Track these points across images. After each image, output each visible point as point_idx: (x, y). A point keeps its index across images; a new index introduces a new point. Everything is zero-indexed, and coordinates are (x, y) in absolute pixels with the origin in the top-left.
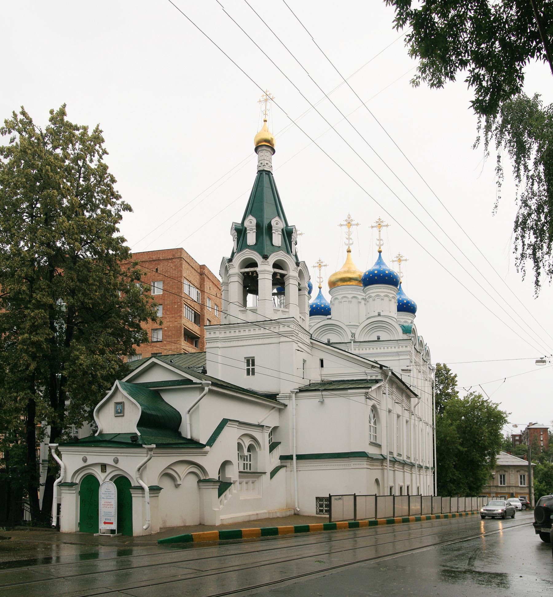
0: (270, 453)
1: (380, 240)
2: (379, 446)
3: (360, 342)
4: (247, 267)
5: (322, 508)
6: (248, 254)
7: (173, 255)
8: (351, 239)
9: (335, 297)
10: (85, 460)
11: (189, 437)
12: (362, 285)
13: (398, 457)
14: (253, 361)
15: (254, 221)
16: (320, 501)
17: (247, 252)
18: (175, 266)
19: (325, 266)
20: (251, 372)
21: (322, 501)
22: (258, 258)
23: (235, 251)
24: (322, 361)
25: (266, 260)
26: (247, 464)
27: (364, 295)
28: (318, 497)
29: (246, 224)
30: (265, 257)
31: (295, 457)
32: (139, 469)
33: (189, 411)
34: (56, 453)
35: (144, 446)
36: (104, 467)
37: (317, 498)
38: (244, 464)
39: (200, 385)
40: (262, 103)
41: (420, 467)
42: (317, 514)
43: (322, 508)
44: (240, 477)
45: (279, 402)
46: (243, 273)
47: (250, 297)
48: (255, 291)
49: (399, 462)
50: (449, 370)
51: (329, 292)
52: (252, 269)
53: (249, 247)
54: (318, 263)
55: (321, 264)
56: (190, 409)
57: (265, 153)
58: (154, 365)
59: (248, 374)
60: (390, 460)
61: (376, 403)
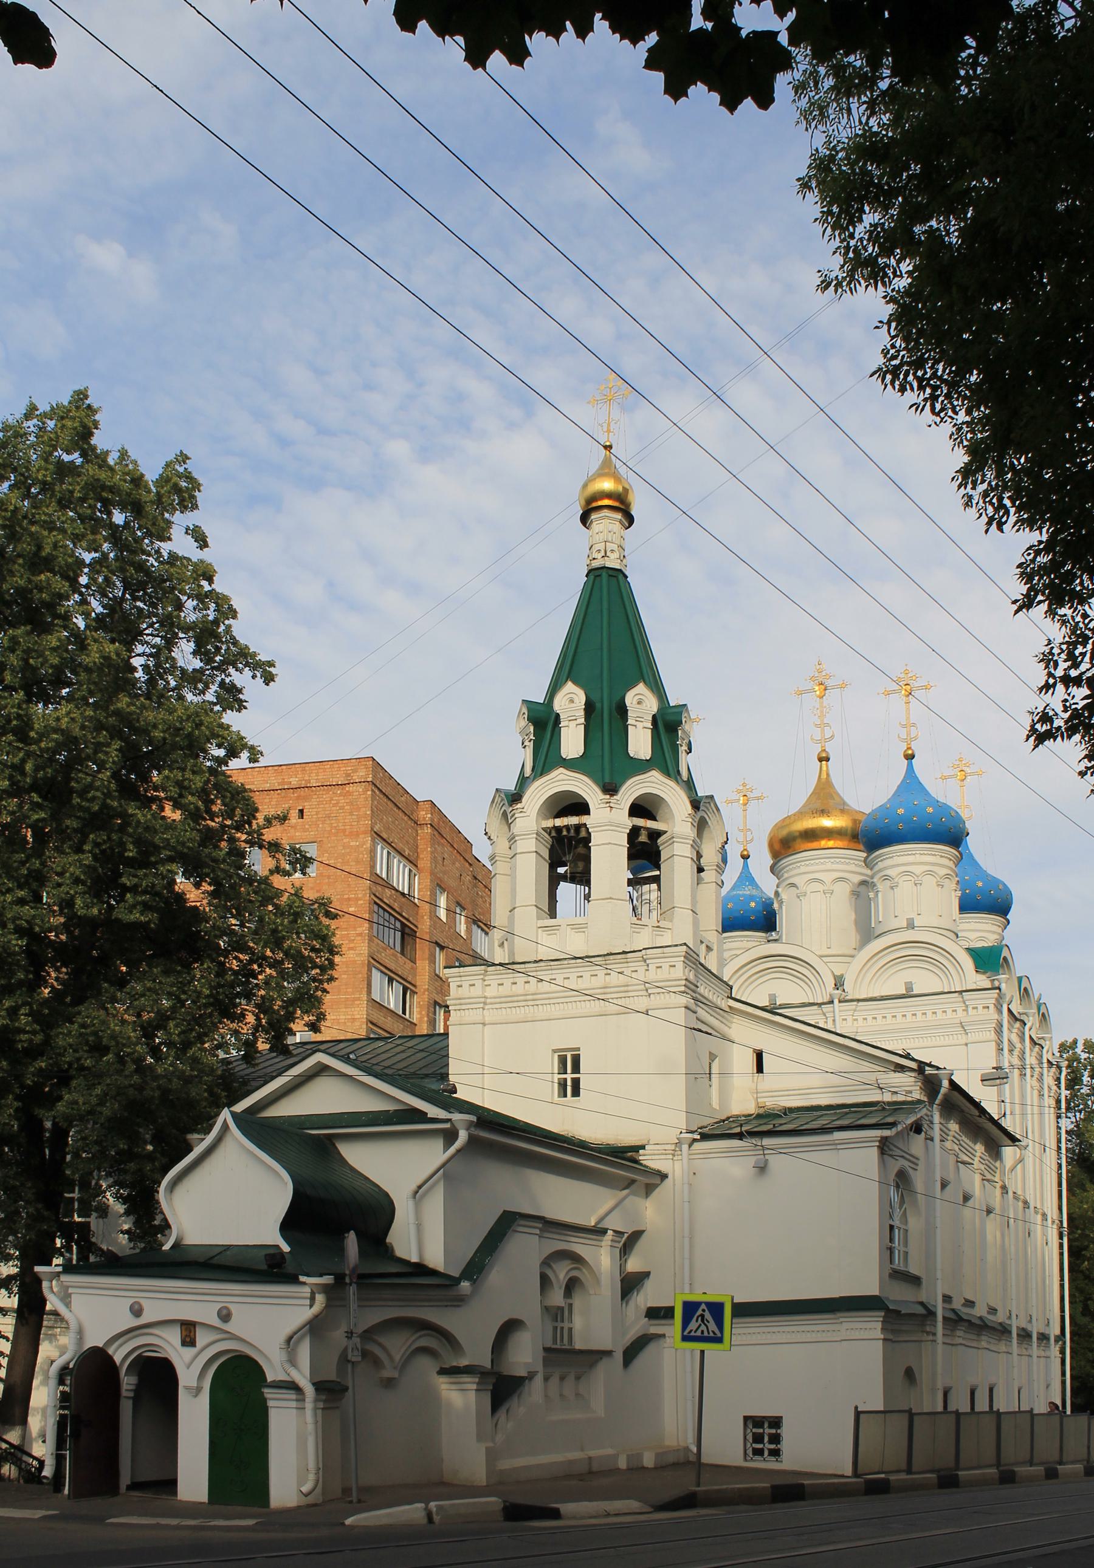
0: (623, 1298)
1: (908, 725)
2: (915, 1281)
3: (859, 1000)
4: (558, 815)
5: (760, 1446)
6: (561, 781)
7: (348, 775)
8: (828, 725)
9: (789, 881)
10: (137, 1311)
11: (414, 1259)
12: (862, 847)
13: (991, 1317)
14: (576, 1061)
15: (580, 697)
17: (562, 777)
18: (351, 803)
19: (758, 798)
20: (569, 1089)
21: (762, 1426)
22: (585, 788)
23: (528, 772)
24: (759, 1056)
25: (612, 795)
26: (562, 1328)
27: (869, 872)
28: (751, 1417)
29: (560, 704)
30: (610, 789)
32: (289, 1340)
33: (416, 1192)
35: (302, 1278)
36: (189, 1331)
38: (555, 1328)
40: (600, 406)
41: (1025, 1335)
42: (745, 1460)
43: (760, 1446)
44: (546, 1362)
45: (645, 1166)
47: (566, 890)
48: (582, 877)
49: (969, 1321)
51: (772, 869)
52: (573, 820)
53: (571, 764)
54: (739, 791)
55: (748, 794)
56: (420, 1187)
57: (606, 523)
58: (321, 1070)
60: (944, 1318)
61: (906, 1164)
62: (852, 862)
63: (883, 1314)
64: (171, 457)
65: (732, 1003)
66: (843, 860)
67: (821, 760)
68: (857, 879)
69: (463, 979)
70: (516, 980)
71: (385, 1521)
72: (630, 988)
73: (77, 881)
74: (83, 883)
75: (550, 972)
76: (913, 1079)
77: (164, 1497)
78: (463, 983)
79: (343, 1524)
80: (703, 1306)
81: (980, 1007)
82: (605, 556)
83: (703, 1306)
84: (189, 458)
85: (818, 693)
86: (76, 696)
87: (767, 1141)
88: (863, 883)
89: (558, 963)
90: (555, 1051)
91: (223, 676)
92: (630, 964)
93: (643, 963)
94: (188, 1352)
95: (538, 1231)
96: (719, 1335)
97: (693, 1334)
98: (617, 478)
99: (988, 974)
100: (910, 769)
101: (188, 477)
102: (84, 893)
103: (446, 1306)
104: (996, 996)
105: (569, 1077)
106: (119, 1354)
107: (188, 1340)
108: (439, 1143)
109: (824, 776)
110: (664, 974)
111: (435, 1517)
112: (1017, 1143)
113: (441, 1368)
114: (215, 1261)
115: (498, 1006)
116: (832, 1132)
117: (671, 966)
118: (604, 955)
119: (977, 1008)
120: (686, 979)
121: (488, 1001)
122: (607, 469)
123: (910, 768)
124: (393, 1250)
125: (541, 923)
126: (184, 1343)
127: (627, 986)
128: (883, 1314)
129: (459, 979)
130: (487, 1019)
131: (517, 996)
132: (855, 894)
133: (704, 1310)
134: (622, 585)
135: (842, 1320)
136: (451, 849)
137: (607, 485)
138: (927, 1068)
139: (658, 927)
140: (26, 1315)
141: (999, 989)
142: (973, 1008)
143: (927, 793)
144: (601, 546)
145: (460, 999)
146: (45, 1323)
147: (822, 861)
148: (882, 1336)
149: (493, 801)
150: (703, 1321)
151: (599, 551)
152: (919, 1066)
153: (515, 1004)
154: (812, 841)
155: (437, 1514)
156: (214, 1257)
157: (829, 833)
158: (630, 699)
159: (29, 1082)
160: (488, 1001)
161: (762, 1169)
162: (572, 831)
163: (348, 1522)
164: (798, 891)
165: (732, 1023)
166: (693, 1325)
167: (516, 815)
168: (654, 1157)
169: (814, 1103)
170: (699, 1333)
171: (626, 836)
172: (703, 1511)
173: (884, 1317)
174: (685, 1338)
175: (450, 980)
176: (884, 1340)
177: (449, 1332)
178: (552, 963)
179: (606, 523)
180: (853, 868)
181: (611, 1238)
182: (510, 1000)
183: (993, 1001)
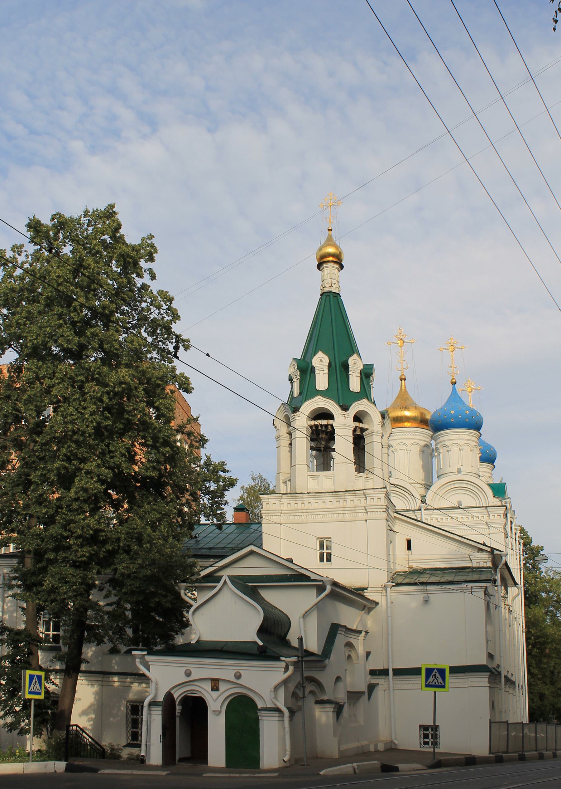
8: (405, 361)
10: (188, 674)
15: (326, 360)
16: (424, 730)
17: (320, 400)
22: (331, 406)
24: (409, 542)
25: (346, 411)
30: (345, 408)
31: (391, 672)
33: (304, 615)
34: (141, 663)
35: (282, 658)
36: (215, 684)
37: (420, 726)
39: (321, 583)
42: (420, 747)
46: (311, 427)
50: (203, 441)
52: (324, 422)
53: (323, 393)
56: (306, 613)
57: (330, 269)
59: (322, 560)
62: (420, 434)
63: (489, 674)
64: (146, 236)
65: (396, 515)
66: (416, 433)
67: (401, 380)
68: (423, 443)
69: (270, 500)
70: (297, 502)
71: (337, 773)
72: (357, 508)
73: (123, 455)
74: (125, 456)
75: (315, 499)
76: (487, 556)
77: (199, 765)
78: (270, 503)
79: (319, 774)
80: (436, 670)
81: (496, 515)
82: (331, 286)
83: (436, 670)
84: (154, 237)
85: (399, 344)
86: (122, 363)
87: (429, 587)
88: (426, 446)
89: (320, 494)
90: (318, 538)
91: (164, 346)
92: (357, 496)
93: (363, 496)
94: (215, 694)
95: (343, 633)
96: (443, 684)
97: (431, 684)
98: (335, 245)
99: (500, 499)
100: (454, 390)
101: (153, 246)
102: (125, 461)
103: (320, 670)
104: (504, 510)
105: (325, 551)
106: (177, 695)
107: (215, 688)
108: (314, 592)
109: (403, 388)
110: (376, 502)
111: (356, 770)
112: (517, 586)
113: (316, 701)
114: (225, 648)
115: (288, 515)
116: (461, 584)
117: (378, 498)
118: (344, 492)
119: (494, 516)
120: (386, 506)
121: (283, 512)
122: (330, 241)
123: (454, 389)
124: (290, 643)
125: (309, 473)
126: (213, 689)
127: (356, 507)
128: (489, 674)
129: (267, 500)
130: (282, 522)
131: (298, 510)
132: (422, 451)
133: (436, 672)
134: (339, 299)
135: (468, 677)
136: (182, 410)
137: (331, 250)
138: (495, 551)
139: (367, 477)
140: (72, 673)
141: (506, 506)
142: (493, 516)
143: (464, 403)
144: (329, 281)
145: (268, 510)
146: (79, 678)
147: (405, 433)
148: (488, 685)
149: (279, 409)
150: (435, 677)
151: (328, 283)
152: (491, 550)
153: (297, 514)
154: (400, 423)
155: (358, 769)
156: (223, 647)
157: (408, 419)
158: (351, 361)
159: (101, 556)
160: (283, 512)
161: (426, 601)
162: (324, 427)
163: (322, 773)
164: (393, 449)
165: (395, 524)
166: (431, 679)
167: (296, 418)
168: (372, 594)
169: (437, 566)
170: (433, 683)
171: (352, 431)
172: (444, 769)
173: (489, 676)
174: (427, 686)
175: (262, 500)
176: (489, 687)
177: (321, 683)
178: (317, 494)
179: (330, 269)
180: (420, 438)
181: (364, 635)
182: (294, 512)
183: (503, 512)
